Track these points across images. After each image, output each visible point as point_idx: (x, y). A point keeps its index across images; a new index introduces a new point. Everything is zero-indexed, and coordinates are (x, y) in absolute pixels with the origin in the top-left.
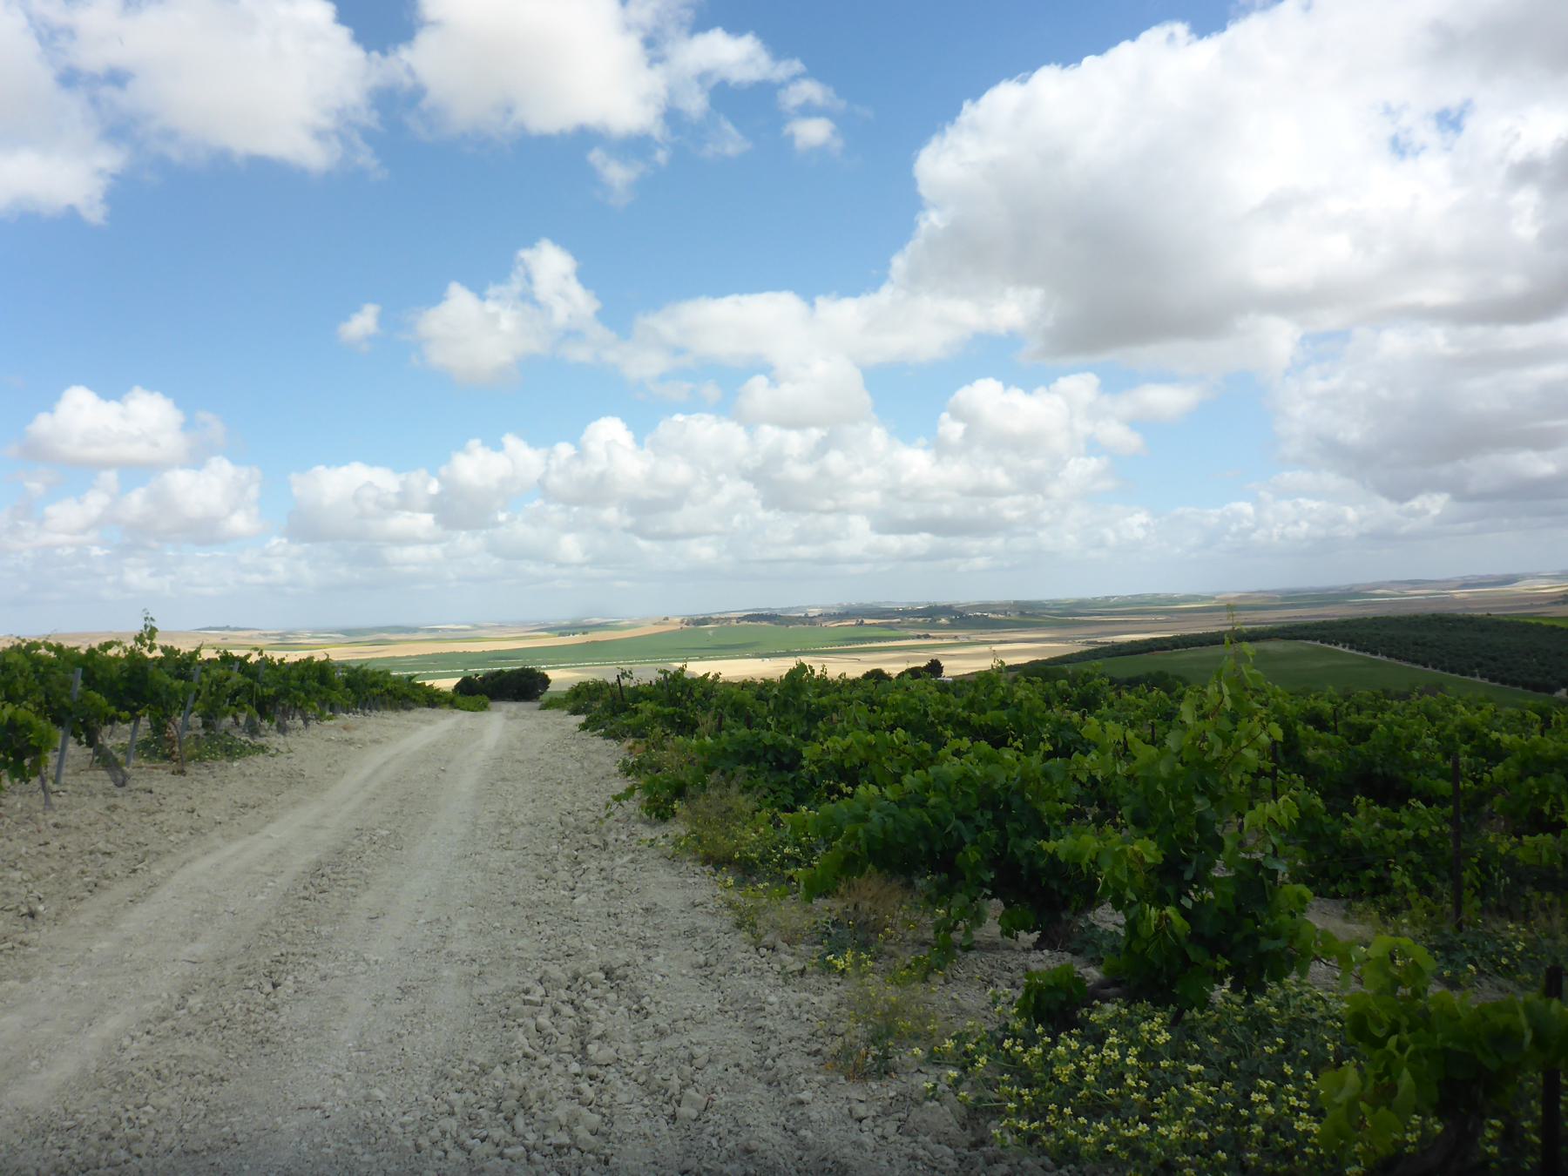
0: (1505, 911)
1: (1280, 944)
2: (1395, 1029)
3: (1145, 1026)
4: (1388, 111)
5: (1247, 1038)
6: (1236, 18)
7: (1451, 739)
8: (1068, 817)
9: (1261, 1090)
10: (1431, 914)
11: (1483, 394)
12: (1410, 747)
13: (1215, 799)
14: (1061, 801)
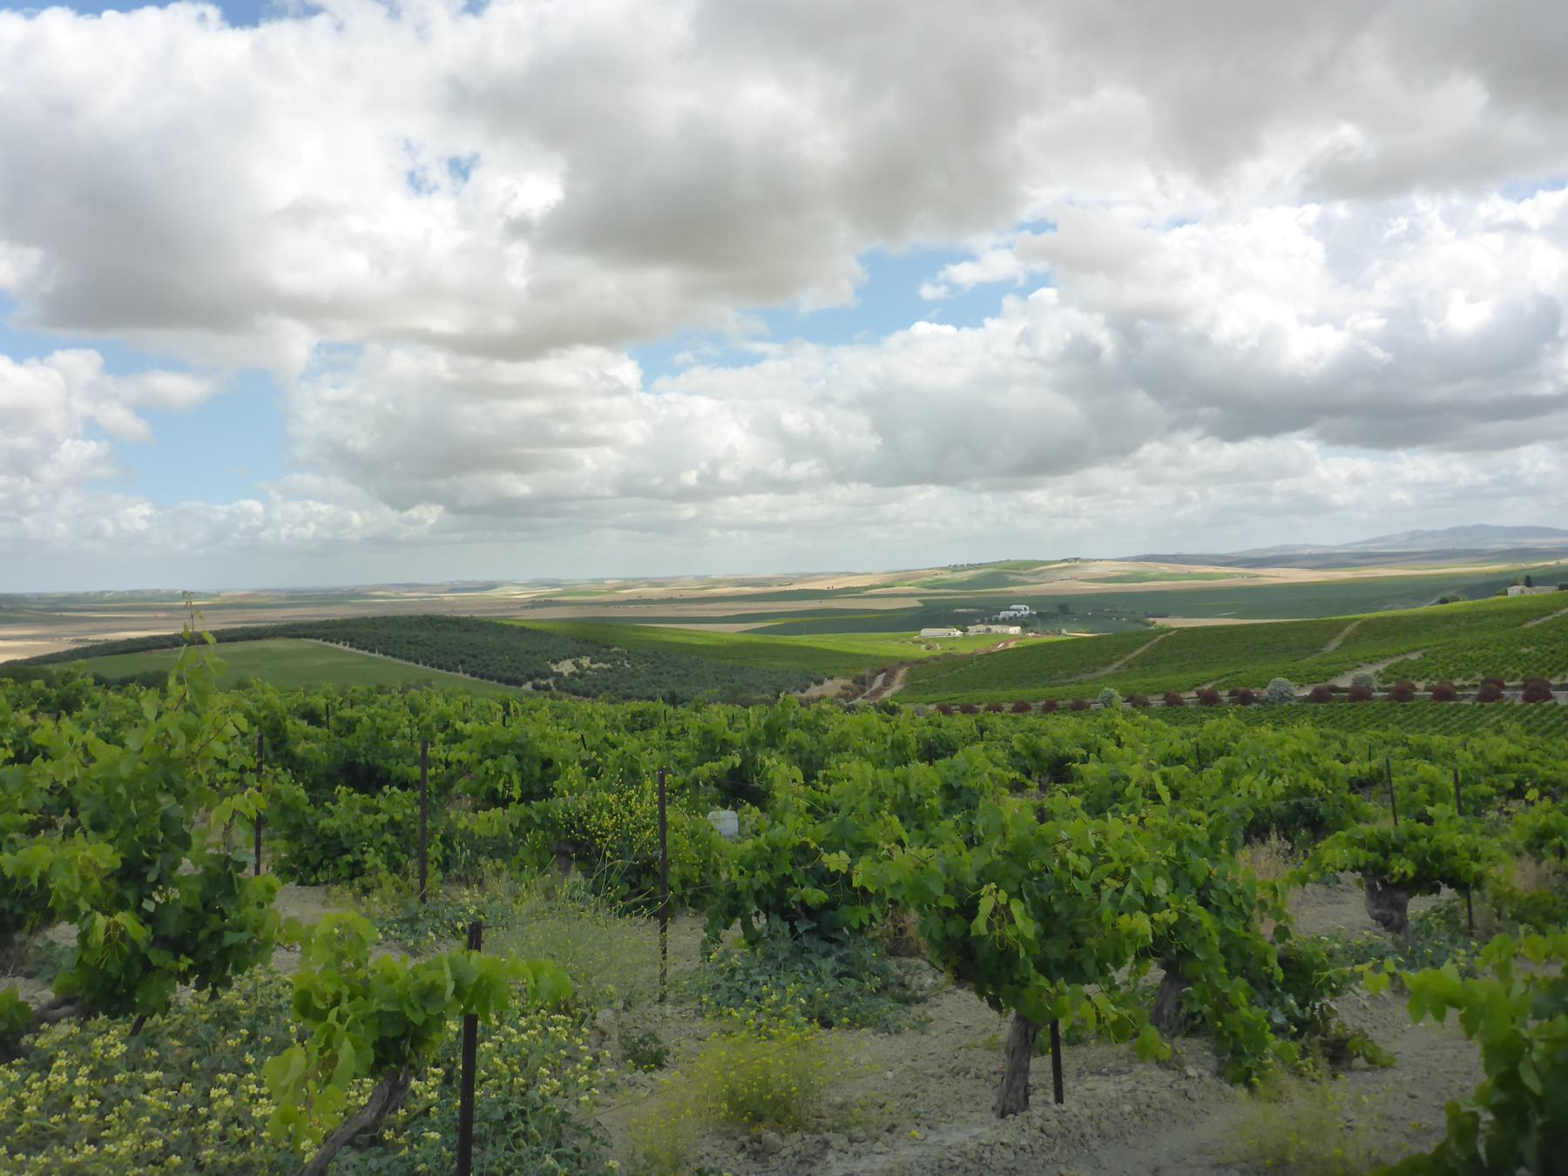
0: (463, 881)
1: (244, 936)
2: (336, 1002)
3: (98, 1042)
4: (408, 146)
5: (210, 1034)
6: (269, 18)
7: (428, 728)
8: (32, 830)
9: (221, 1085)
10: (399, 890)
11: (473, 418)
12: (390, 737)
13: (181, 795)
14: (22, 812)
